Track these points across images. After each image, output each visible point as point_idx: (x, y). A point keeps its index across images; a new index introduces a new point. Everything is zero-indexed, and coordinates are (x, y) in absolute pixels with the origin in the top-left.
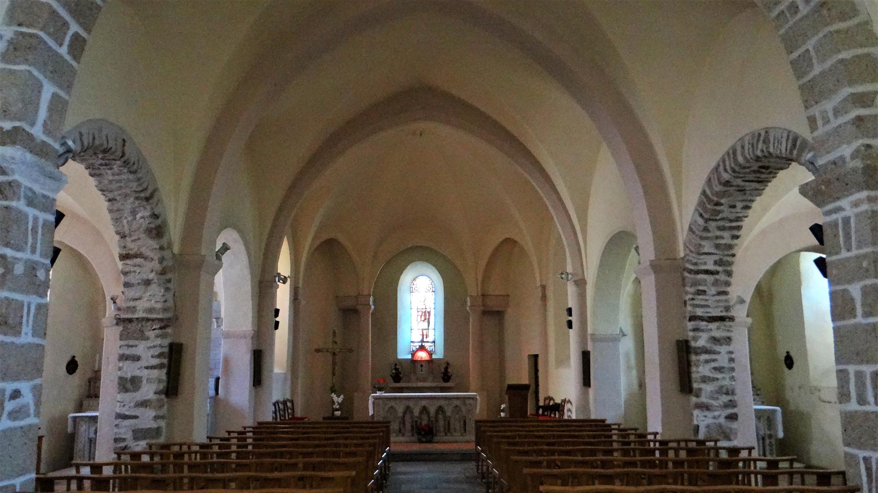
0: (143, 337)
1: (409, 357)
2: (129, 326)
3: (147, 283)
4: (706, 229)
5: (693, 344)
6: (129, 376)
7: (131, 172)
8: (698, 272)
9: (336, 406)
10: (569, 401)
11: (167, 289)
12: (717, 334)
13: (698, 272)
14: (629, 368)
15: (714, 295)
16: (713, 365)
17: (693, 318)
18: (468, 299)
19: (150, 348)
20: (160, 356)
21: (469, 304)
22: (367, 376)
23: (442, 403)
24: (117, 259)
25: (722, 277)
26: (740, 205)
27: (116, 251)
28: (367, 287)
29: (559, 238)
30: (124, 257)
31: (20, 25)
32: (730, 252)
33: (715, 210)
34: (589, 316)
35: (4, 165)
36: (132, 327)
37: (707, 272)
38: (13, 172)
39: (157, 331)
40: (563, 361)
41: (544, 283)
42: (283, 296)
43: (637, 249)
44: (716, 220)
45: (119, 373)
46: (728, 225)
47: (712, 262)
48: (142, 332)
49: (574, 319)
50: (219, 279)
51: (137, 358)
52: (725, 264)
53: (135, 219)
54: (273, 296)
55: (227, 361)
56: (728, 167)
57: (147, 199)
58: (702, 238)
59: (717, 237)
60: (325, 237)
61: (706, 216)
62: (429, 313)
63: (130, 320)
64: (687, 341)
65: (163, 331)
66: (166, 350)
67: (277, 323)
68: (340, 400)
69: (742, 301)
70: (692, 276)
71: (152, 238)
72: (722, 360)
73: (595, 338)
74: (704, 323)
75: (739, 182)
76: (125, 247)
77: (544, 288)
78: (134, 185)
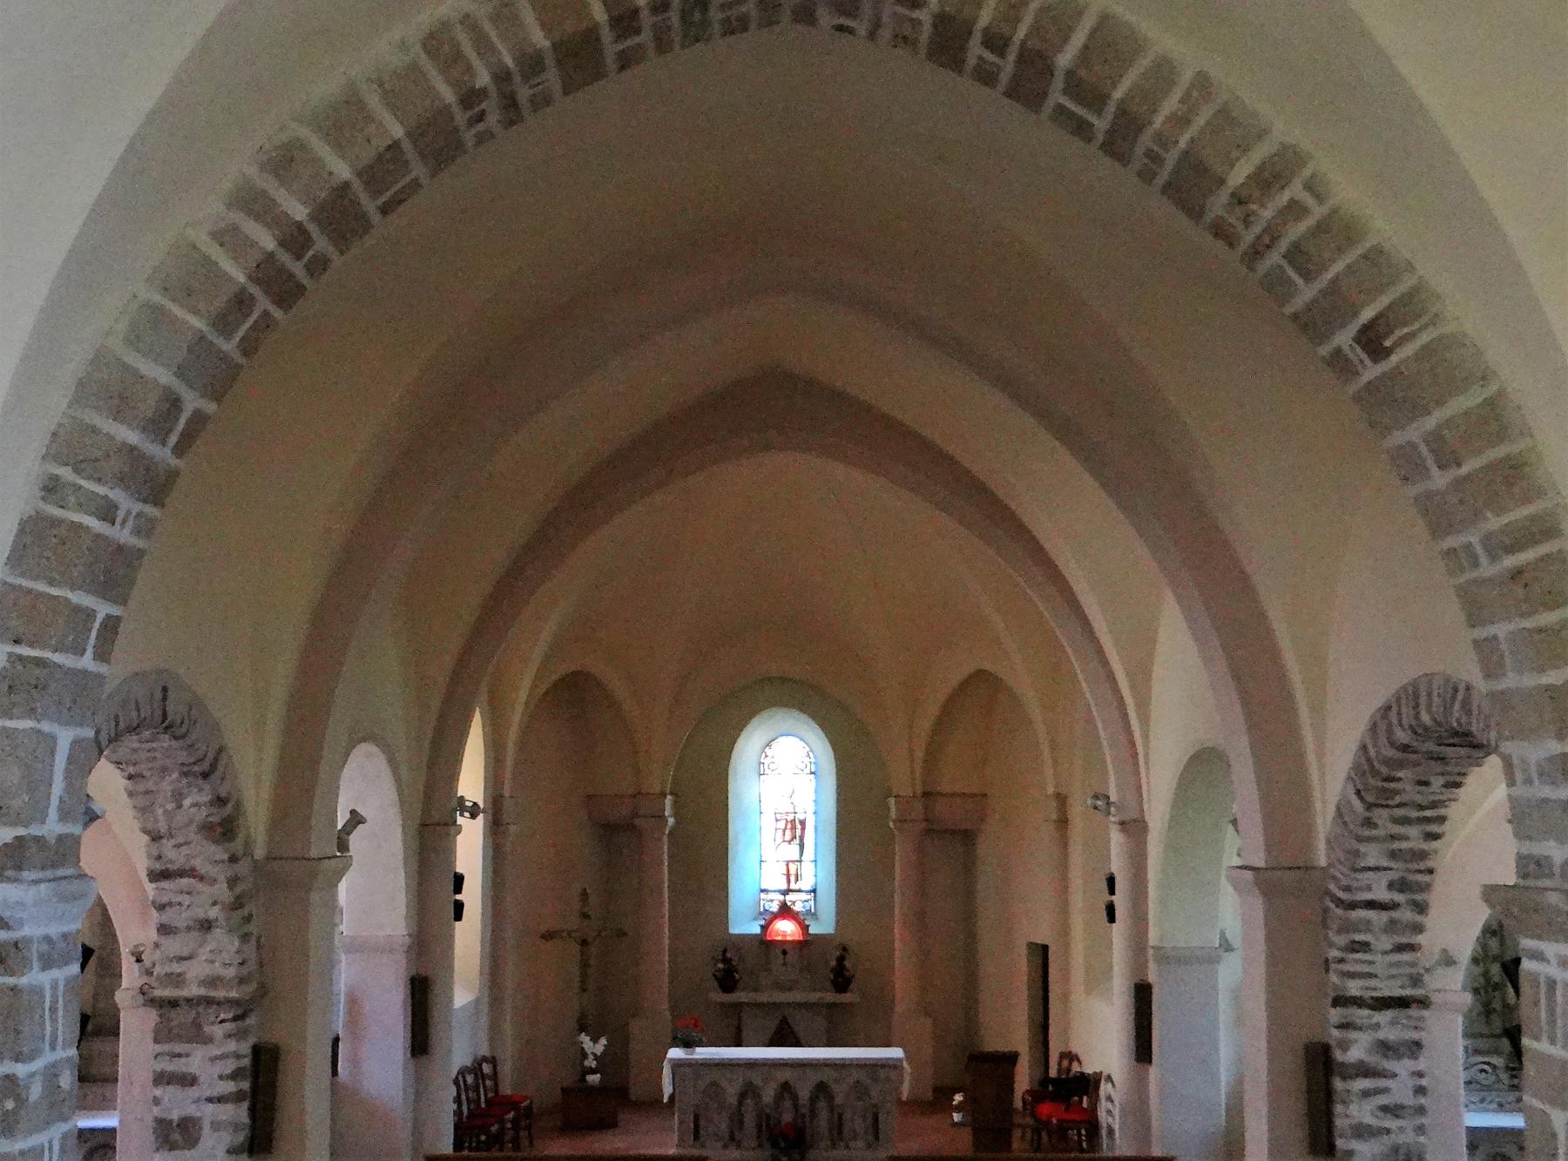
0: (202, 1039)
1: (757, 930)
2: (173, 1013)
3: (206, 926)
4: (1368, 823)
5: (1339, 1056)
6: (175, 1116)
7: (176, 738)
8: (1353, 906)
9: (591, 1063)
10: (1109, 1078)
11: (245, 938)
12: (1391, 1035)
13: (1353, 906)
14: (1239, 1021)
15: (1386, 953)
16: (1382, 1100)
17: (1340, 1001)
18: (892, 801)
19: (214, 1062)
20: (235, 1075)
21: (893, 813)
22: (658, 998)
23: (827, 1075)
24: (145, 879)
25: (1406, 915)
26: (1437, 782)
27: (142, 864)
28: (658, 777)
29: (1090, 720)
30: (157, 876)
31: (17, 642)
32: (1422, 866)
33: (1384, 790)
34: (1151, 905)
35: (7, 914)
36: (181, 1017)
37: (1371, 905)
38: (21, 923)
39: (228, 1026)
40: (1098, 979)
41: (1064, 791)
42: (469, 847)
43: (1234, 822)
44: (1387, 806)
45: (156, 1111)
46: (1414, 814)
47: (1384, 883)
48: (199, 1027)
49: (1119, 900)
50: (342, 887)
51: (188, 1081)
52: (1414, 887)
53: (180, 806)
54: (450, 853)
55: (353, 1002)
56: (1405, 721)
57: (205, 776)
58: (1360, 839)
59: (1393, 837)
60: (563, 669)
61: (1370, 799)
62: (803, 823)
63: (174, 1003)
64: (1326, 1049)
65: (240, 1023)
66: (246, 1062)
67: (459, 908)
68: (599, 1048)
69: (1448, 961)
70: (1339, 911)
71: (216, 842)
72: (1400, 1091)
73: (1164, 958)
74: (1366, 1012)
75: (1430, 746)
76: (160, 857)
77: (1062, 799)
78: (183, 756)
